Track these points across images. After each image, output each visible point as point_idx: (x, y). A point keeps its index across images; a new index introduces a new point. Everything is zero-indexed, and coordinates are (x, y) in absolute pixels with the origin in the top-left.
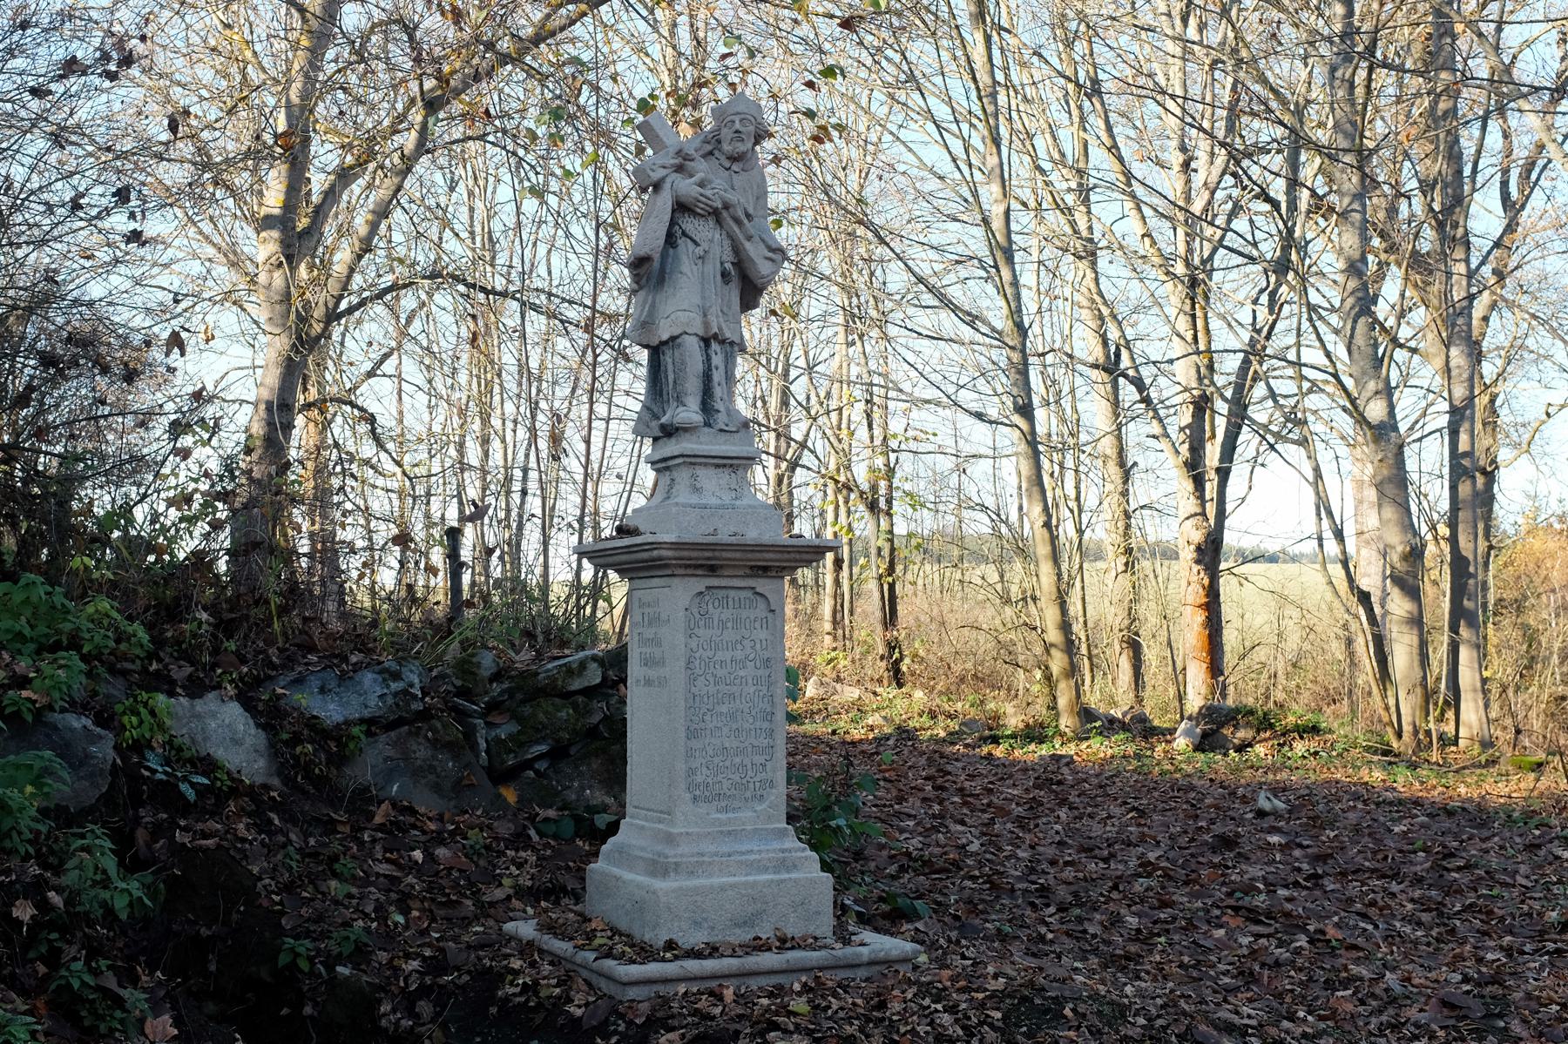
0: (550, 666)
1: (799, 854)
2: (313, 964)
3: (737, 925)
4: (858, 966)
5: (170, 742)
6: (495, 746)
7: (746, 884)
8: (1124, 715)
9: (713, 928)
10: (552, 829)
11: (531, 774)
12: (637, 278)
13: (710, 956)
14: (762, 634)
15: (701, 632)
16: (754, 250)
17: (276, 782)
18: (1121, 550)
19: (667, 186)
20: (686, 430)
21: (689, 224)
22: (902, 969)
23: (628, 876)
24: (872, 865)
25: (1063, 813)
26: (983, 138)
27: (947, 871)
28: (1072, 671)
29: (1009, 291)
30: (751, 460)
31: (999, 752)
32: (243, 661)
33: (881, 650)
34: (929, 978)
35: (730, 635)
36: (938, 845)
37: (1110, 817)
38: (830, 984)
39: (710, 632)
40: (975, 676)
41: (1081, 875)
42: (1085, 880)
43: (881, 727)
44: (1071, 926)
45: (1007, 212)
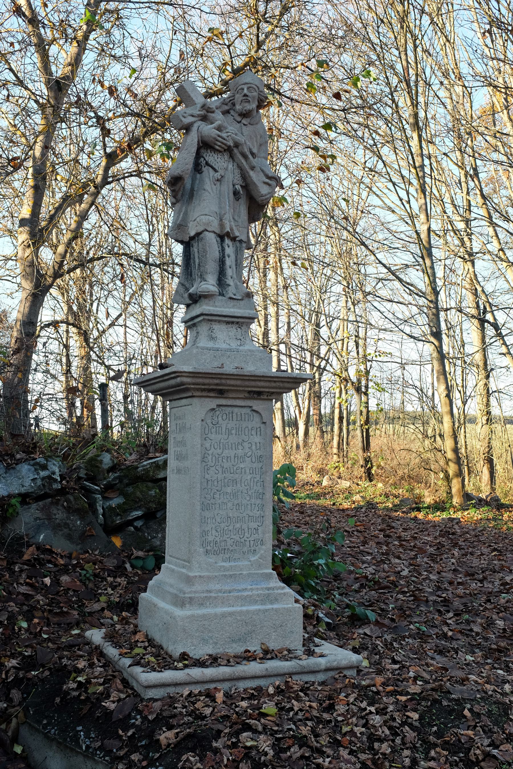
0: (145, 463)
1: (280, 591)
4: (318, 672)
6: (109, 512)
7: (241, 613)
8: (487, 497)
9: (216, 643)
10: (140, 563)
12: (175, 194)
13: (211, 665)
14: (257, 439)
15: (213, 436)
16: (256, 177)
18: (485, 413)
19: (195, 128)
21: (211, 157)
22: (348, 673)
23: (162, 604)
24: (345, 583)
25: (456, 552)
26: (417, 190)
28: (460, 474)
29: (429, 271)
30: (252, 319)
31: (420, 516)
33: (362, 462)
35: (234, 439)
36: (384, 571)
37: (482, 554)
38: (296, 687)
40: (409, 476)
41: (468, 592)
43: (359, 502)
44: (463, 626)
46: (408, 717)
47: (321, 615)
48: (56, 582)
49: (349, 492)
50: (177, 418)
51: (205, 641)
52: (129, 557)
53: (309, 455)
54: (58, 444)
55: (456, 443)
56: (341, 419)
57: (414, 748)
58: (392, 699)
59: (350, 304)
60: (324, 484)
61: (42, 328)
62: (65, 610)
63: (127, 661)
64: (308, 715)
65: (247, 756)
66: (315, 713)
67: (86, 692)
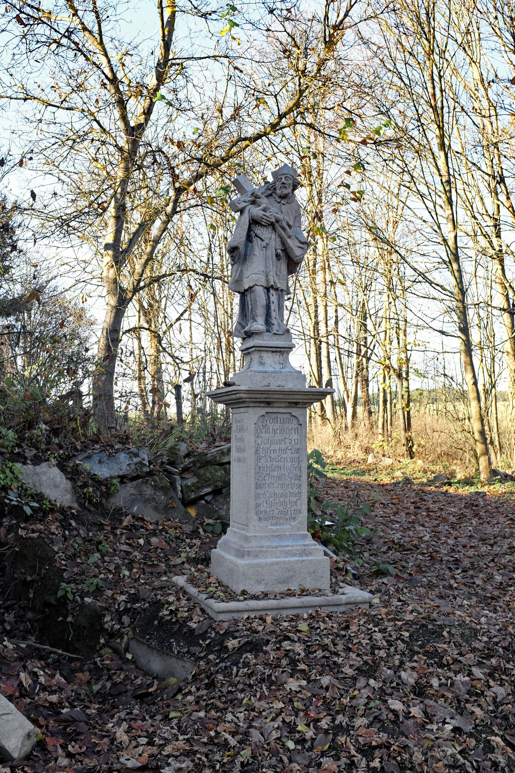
1: (313, 547)
2: (75, 596)
3: (279, 583)
5: (22, 487)
7: (284, 562)
10: (210, 529)
11: (203, 502)
12: (233, 258)
14: (295, 436)
15: (263, 435)
16: (292, 243)
17: (76, 505)
19: (246, 211)
20: (256, 334)
21: (259, 230)
22: (363, 606)
23: (228, 556)
27: (411, 550)
31: (452, 490)
32: (61, 447)
33: (404, 441)
34: (376, 612)
36: (409, 537)
38: (323, 615)
39: (268, 435)
41: (476, 553)
42: (478, 556)
43: (397, 478)
44: (468, 580)
45: (456, 237)
46: (401, 635)
47: (349, 568)
48: (148, 542)
49: (391, 468)
50: (238, 421)
51: (259, 582)
52: (202, 524)
53: (356, 435)
54: (144, 435)
55: (483, 425)
56: (385, 401)
57: (403, 654)
58: (392, 623)
59: (391, 300)
60: (369, 462)
61: (124, 333)
62: (156, 563)
63: (205, 596)
64: (330, 632)
65: (286, 655)
66: (335, 630)
67: (176, 616)
